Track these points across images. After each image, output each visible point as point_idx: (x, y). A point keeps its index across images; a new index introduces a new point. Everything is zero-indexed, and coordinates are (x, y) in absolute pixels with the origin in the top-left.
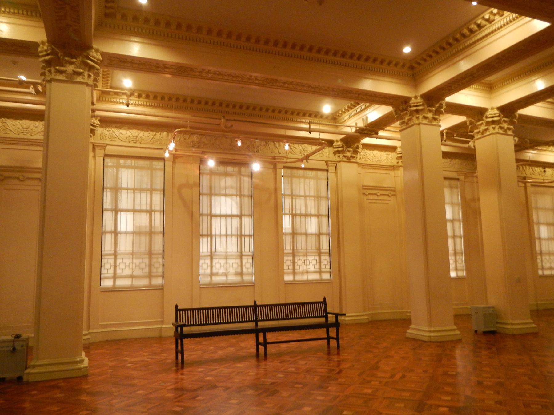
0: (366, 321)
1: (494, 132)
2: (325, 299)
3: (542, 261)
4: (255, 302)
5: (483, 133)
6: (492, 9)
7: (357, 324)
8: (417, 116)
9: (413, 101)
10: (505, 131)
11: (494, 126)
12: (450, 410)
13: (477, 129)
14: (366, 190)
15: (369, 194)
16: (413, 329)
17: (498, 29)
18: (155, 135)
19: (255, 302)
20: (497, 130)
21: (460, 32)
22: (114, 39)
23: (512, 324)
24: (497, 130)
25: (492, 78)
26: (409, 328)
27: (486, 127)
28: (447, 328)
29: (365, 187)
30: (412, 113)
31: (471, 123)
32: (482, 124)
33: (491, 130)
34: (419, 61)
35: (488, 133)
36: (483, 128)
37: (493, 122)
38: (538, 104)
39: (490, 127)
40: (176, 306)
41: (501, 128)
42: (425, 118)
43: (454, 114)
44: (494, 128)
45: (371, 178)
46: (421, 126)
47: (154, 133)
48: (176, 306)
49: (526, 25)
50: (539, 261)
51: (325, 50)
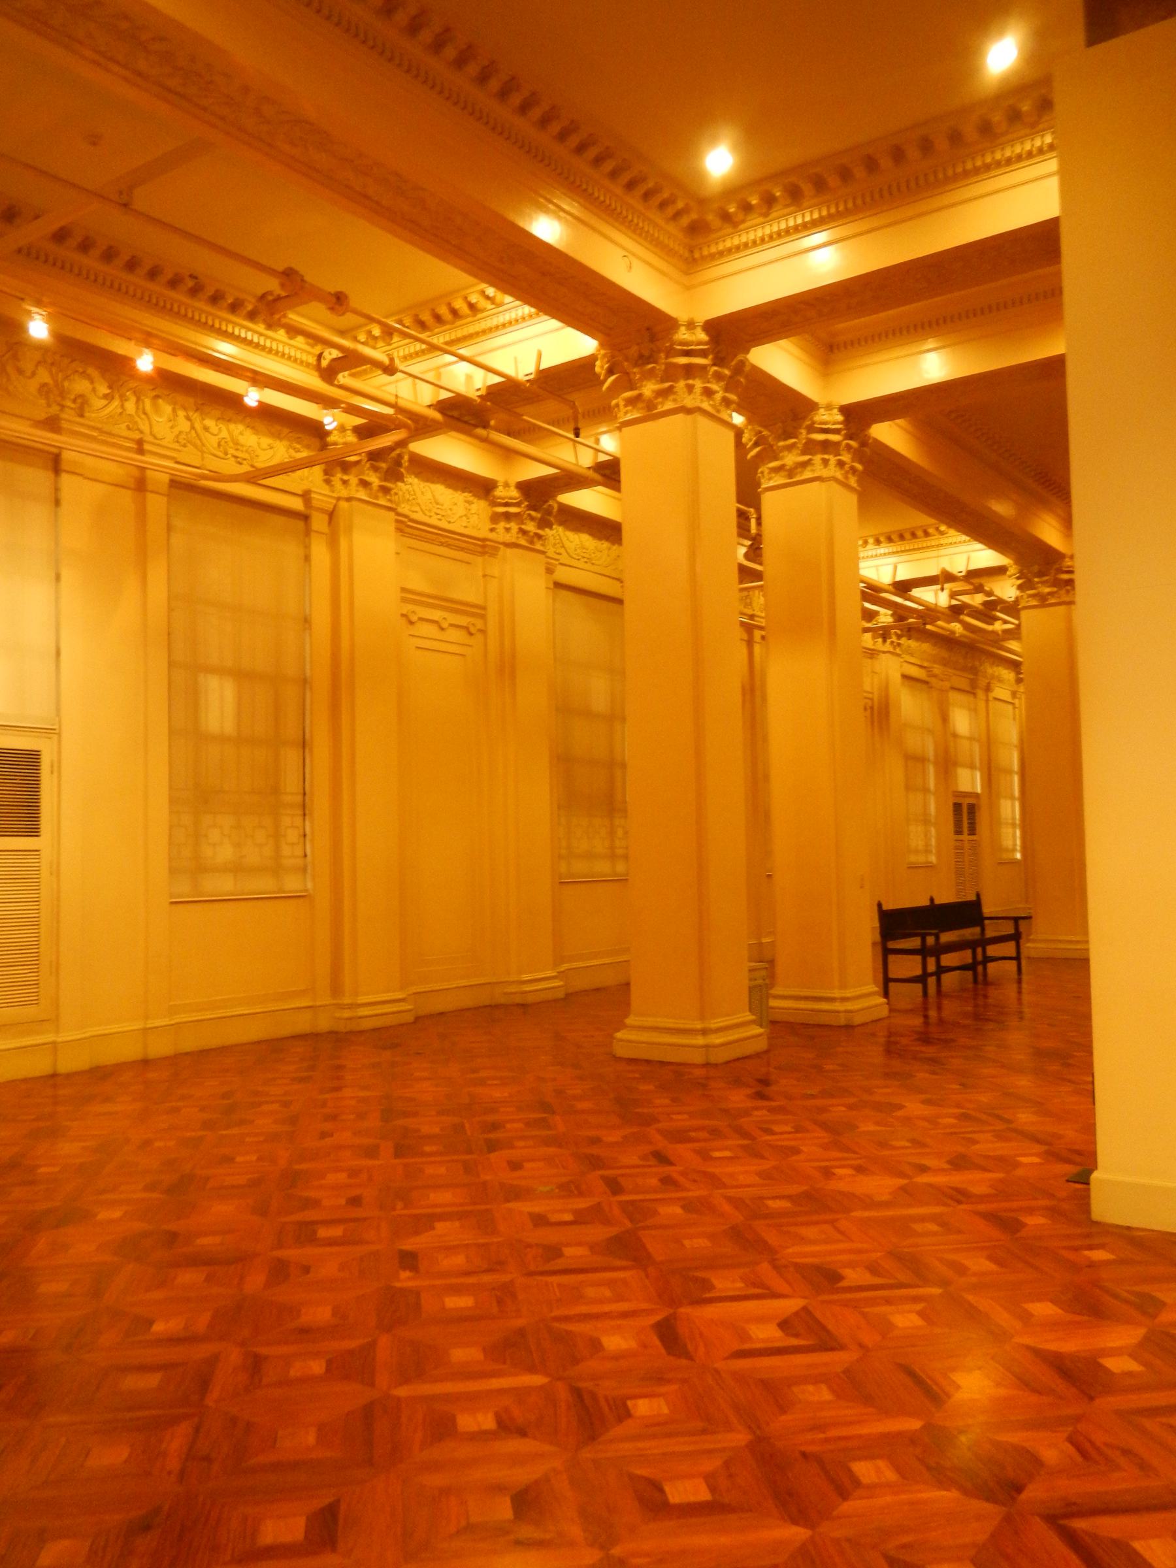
0: (409, 1018)
1: (825, 473)
2: (978, 895)
4: (932, 900)
5: (791, 473)
6: (483, 286)
8: (345, 477)
9: (683, 335)
12: (706, 1285)
13: (776, 458)
16: (634, 1027)
17: (510, 323)
19: (932, 900)
21: (449, 304)
23: (844, 1000)
25: (845, 326)
26: (621, 1026)
27: (806, 458)
28: (682, 1024)
30: (671, 373)
32: (793, 446)
33: (818, 470)
35: (807, 474)
36: (790, 459)
39: (817, 458)
40: (880, 905)
42: (364, 484)
46: (354, 503)
48: (880, 905)
49: (796, 258)
51: (127, 258)
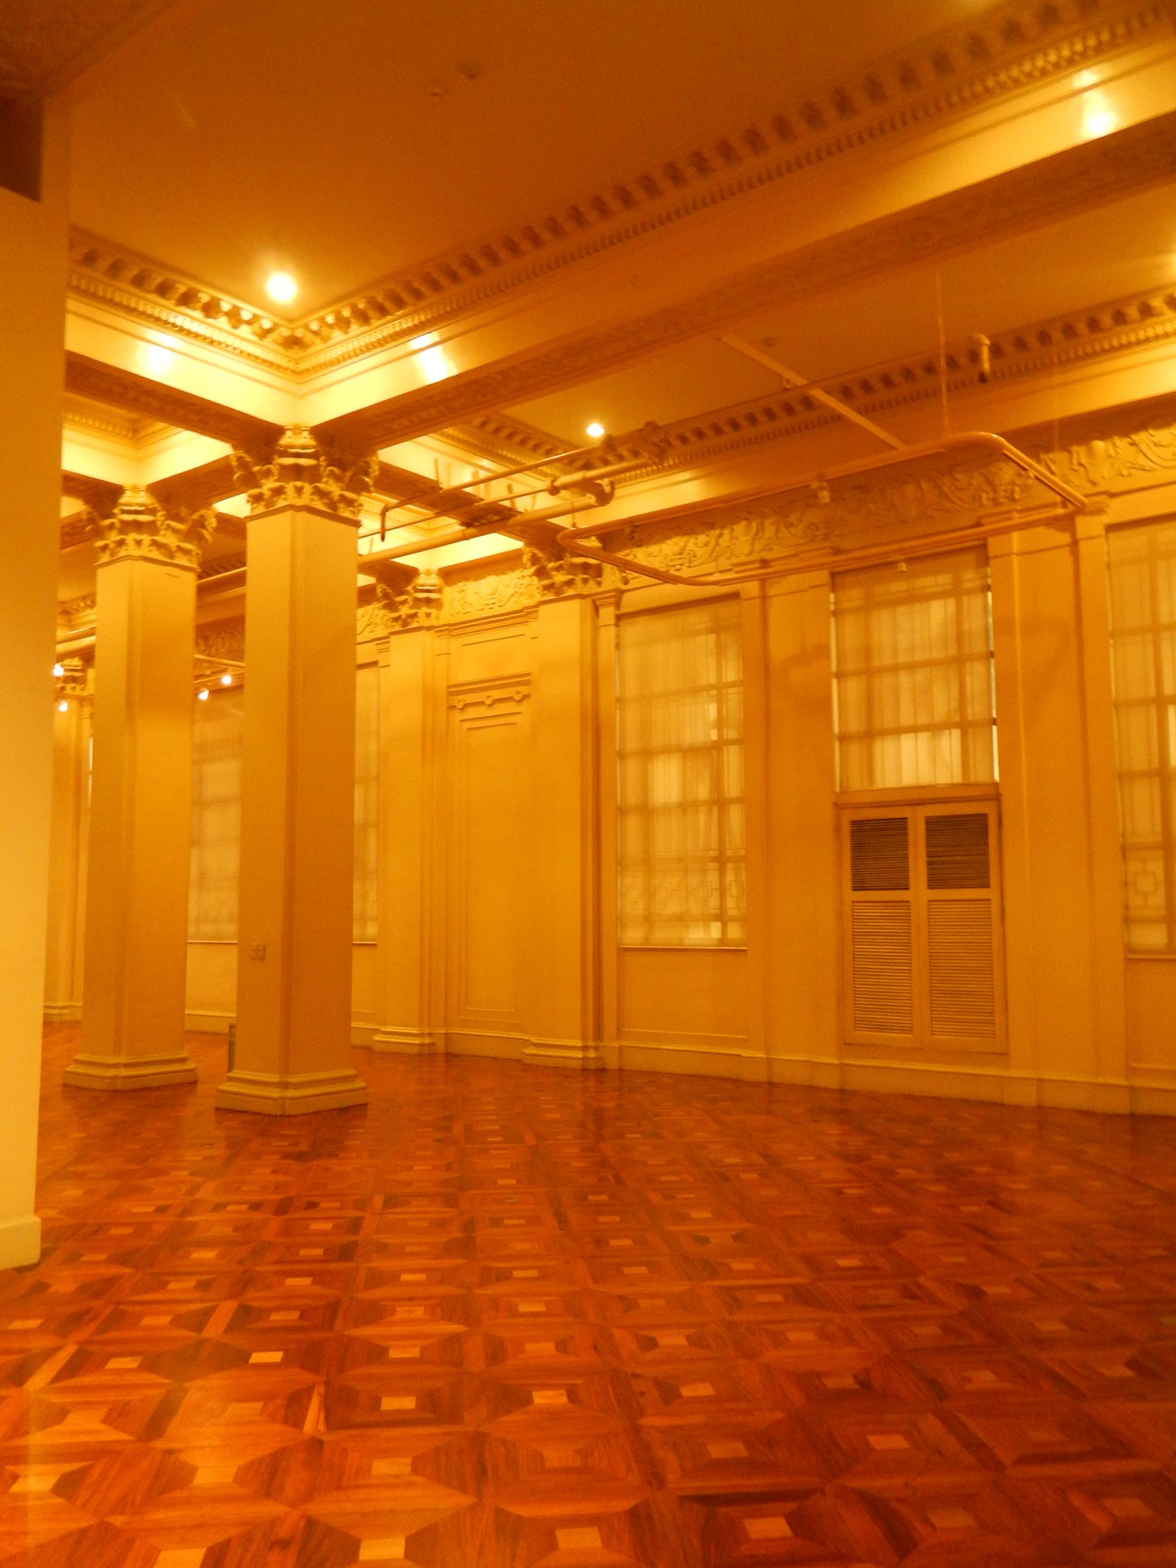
1: (300, 502)
3: (722, 892)
7: (397, 1054)
10: (333, 505)
11: (299, 484)
14: (455, 696)
15: (466, 706)
18: (720, 536)
20: (306, 498)
22: (975, 113)
24: (306, 498)
29: (454, 690)
31: (242, 463)
33: (290, 497)
34: (435, 275)
35: (281, 503)
37: (297, 472)
38: (423, 439)
39: (290, 487)
41: (322, 494)
43: (187, 429)
44: (299, 491)
45: (471, 662)
47: (718, 532)
50: (733, 891)
